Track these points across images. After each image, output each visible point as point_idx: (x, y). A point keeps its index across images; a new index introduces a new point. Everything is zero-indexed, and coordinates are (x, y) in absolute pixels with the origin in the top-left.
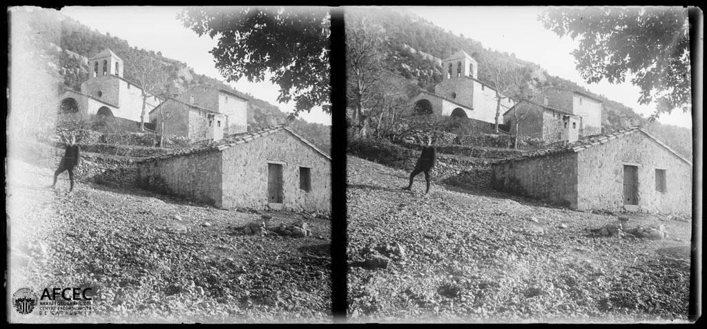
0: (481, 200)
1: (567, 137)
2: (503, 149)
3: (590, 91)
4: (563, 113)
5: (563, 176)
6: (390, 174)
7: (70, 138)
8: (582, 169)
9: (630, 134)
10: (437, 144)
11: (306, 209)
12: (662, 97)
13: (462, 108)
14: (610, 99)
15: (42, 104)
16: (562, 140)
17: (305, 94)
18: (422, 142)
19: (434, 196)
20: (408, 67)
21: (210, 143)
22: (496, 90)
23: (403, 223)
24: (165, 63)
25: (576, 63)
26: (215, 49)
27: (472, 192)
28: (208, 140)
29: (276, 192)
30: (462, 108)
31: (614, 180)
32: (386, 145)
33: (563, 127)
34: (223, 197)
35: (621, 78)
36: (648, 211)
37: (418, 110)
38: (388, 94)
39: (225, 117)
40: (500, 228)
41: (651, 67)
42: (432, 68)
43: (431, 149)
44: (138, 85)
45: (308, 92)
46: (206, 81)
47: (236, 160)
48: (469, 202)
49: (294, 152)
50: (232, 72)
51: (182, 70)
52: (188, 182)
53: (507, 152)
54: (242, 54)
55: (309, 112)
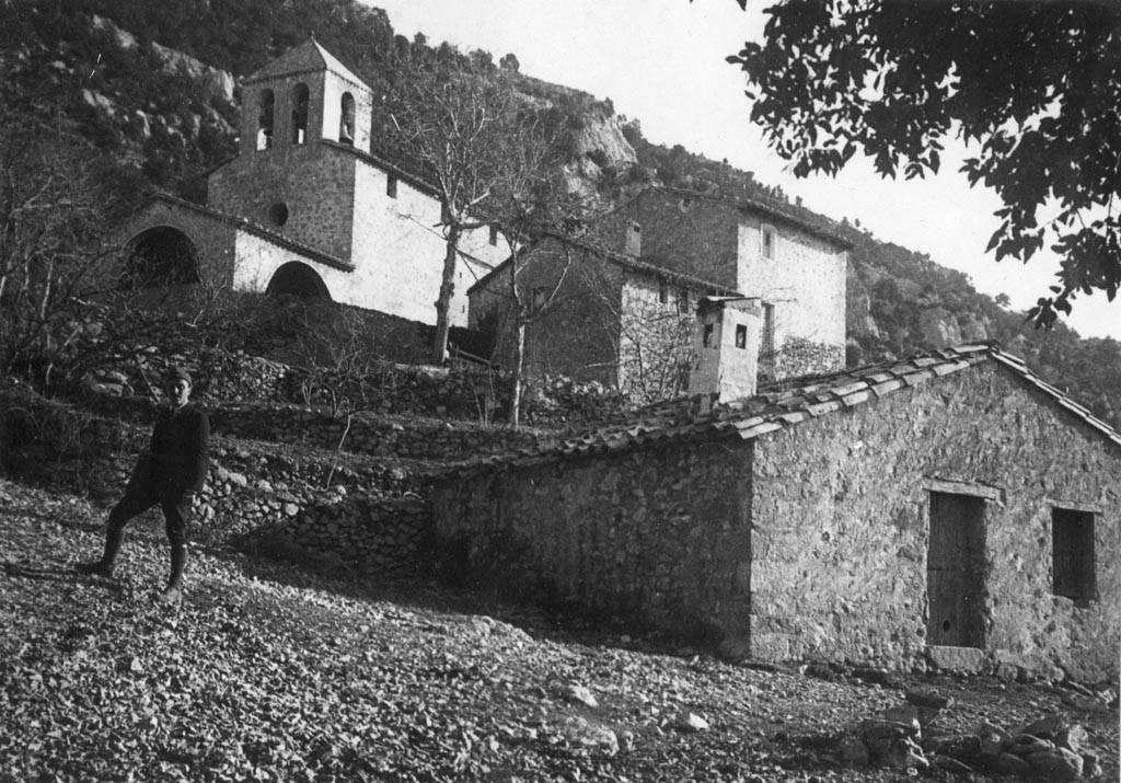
0: (379, 617)
1: (714, 379)
2: (466, 425)
3: (804, 204)
4: (700, 287)
5: (695, 532)
6: (30, 512)
7: (171, 380)
8: (771, 507)
9: (957, 373)
10: (211, 400)
11: (1077, 672)
12: (1085, 232)
13: (311, 263)
14: (882, 235)
15: (61, 249)
16: (694, 390)
17: (1098, 224)
18: (157, 391)
19: (200, 599)
20: (105, 102)
21: (705, 410)
22: (442, 199)
23: (78, 700)
24: (531, 99)
25: (751, 96)
26: (751, 46)
27: (341, 585)
28: (697, 399)
29: (959, 599)
30: (311, 263)
31: (894, 551)
32: (18, 400)
33: (696, 341)
34: (754, 618)
35: (926, 155)
36: (1021, 671)
37: (141, 268)
38: (29, 206)
39: (763, 311)
40: (452, 728)
41: (1043, 114)
42: (200, 111)
43: (191, 417)
44: (427, 184)
45: (1109, 220)
46: (688, 171)
47: (805, 477)
48: (332, 624)
49: (1030, 448)
50: (814, 135)
51: (596, 127)
52: (620, 558)
53: (480, 433)
54: (851, 65)
55: (1111, 296)
